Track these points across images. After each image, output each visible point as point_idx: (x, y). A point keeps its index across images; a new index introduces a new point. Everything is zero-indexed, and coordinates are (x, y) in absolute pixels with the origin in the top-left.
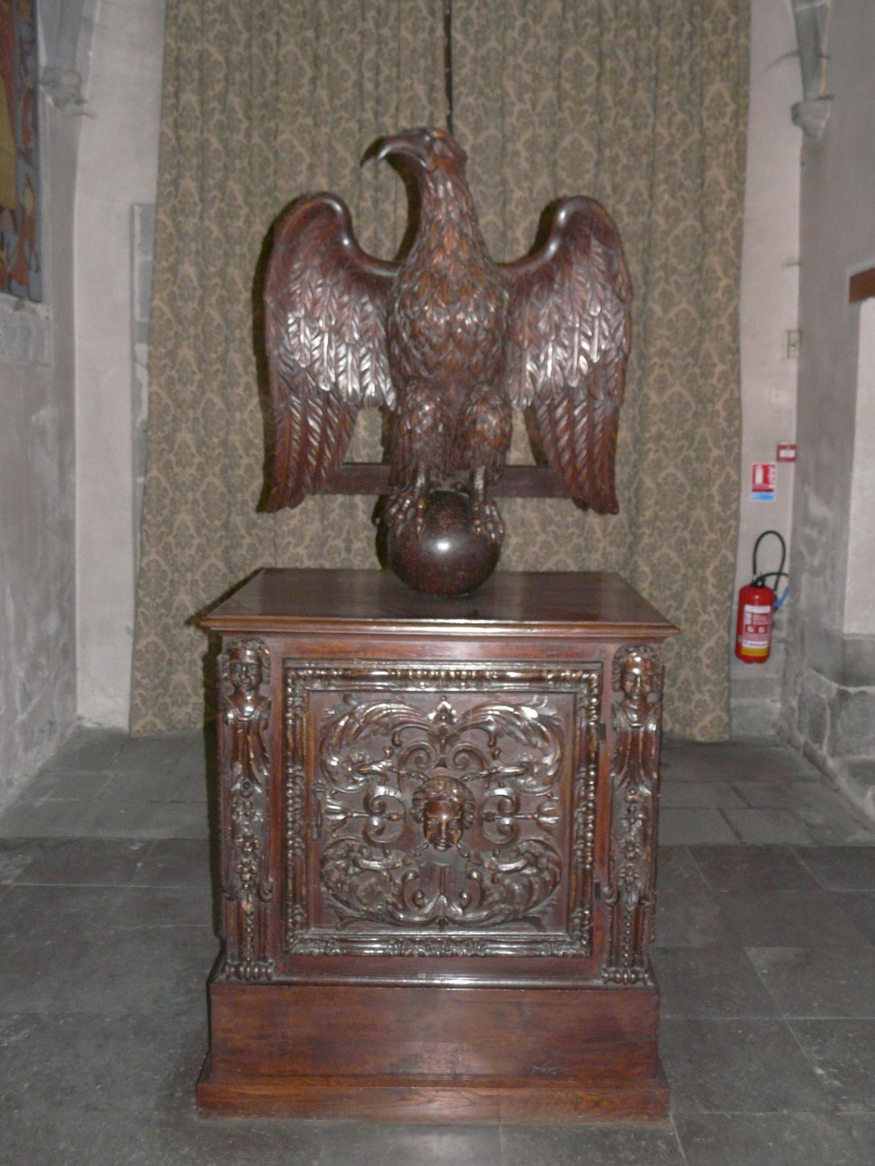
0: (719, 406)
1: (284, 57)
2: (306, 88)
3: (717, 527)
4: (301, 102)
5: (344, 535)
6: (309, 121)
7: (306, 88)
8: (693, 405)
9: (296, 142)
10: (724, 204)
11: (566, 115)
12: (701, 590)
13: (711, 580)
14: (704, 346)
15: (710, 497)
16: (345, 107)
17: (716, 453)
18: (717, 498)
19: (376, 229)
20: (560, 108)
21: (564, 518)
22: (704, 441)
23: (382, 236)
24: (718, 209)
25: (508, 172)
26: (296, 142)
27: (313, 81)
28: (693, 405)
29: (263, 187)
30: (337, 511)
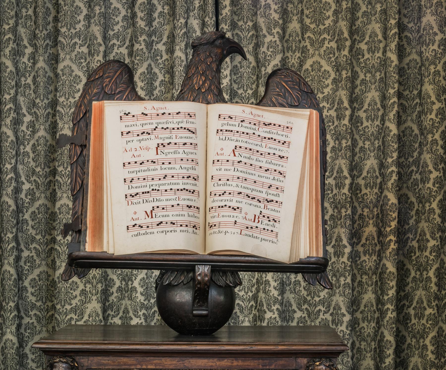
0: (431, 274)
1: (62, 70)
2: (82, 23)
3: (434, 304)
4: (78, 34)
5: (127, 43)
6: (85, 49)
7: (82, 23)
8: (416, 204)
9: (74, 67)
10: (437, 43)
11: (307, 43)
12: (422, 356)
13: (430, 348)
14: (422, 157)
15: (425, 347)
16: (117, 36)
17: (429, 311)
18: (434, 280)
19: (150, 65)
20: (303, 39)
21: (313, 298)
22: (420, 301)
23: (156, 70)
24: (430, 117)
25: (261, 21)
26: (74, 67)
27: (88, 17)
28: (416, 204)
29: (45, 32)
30: (121, 24)
